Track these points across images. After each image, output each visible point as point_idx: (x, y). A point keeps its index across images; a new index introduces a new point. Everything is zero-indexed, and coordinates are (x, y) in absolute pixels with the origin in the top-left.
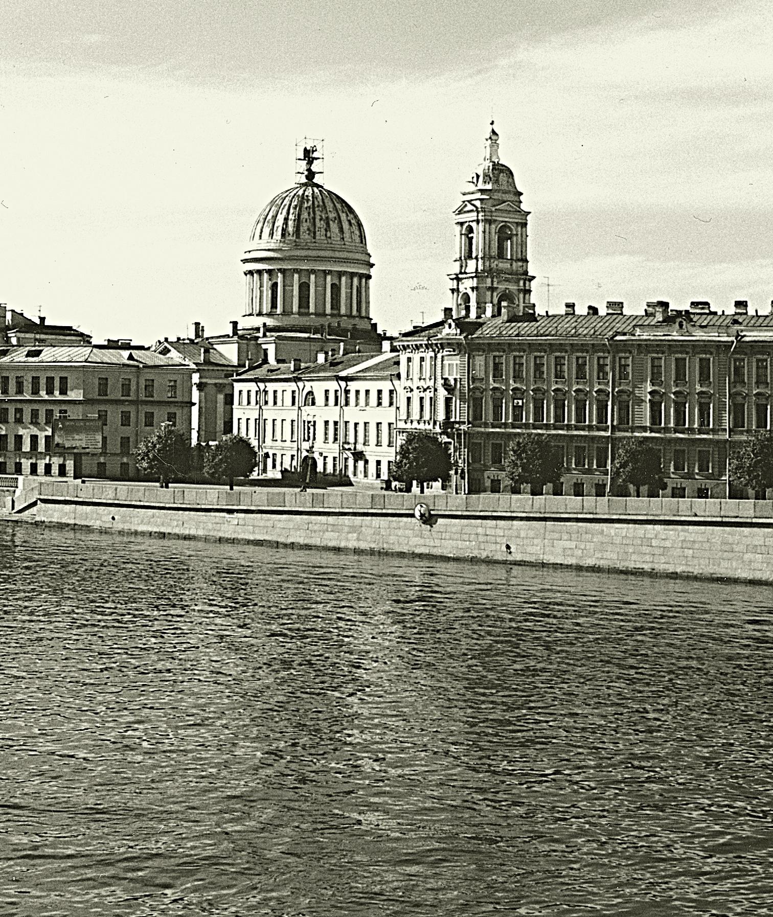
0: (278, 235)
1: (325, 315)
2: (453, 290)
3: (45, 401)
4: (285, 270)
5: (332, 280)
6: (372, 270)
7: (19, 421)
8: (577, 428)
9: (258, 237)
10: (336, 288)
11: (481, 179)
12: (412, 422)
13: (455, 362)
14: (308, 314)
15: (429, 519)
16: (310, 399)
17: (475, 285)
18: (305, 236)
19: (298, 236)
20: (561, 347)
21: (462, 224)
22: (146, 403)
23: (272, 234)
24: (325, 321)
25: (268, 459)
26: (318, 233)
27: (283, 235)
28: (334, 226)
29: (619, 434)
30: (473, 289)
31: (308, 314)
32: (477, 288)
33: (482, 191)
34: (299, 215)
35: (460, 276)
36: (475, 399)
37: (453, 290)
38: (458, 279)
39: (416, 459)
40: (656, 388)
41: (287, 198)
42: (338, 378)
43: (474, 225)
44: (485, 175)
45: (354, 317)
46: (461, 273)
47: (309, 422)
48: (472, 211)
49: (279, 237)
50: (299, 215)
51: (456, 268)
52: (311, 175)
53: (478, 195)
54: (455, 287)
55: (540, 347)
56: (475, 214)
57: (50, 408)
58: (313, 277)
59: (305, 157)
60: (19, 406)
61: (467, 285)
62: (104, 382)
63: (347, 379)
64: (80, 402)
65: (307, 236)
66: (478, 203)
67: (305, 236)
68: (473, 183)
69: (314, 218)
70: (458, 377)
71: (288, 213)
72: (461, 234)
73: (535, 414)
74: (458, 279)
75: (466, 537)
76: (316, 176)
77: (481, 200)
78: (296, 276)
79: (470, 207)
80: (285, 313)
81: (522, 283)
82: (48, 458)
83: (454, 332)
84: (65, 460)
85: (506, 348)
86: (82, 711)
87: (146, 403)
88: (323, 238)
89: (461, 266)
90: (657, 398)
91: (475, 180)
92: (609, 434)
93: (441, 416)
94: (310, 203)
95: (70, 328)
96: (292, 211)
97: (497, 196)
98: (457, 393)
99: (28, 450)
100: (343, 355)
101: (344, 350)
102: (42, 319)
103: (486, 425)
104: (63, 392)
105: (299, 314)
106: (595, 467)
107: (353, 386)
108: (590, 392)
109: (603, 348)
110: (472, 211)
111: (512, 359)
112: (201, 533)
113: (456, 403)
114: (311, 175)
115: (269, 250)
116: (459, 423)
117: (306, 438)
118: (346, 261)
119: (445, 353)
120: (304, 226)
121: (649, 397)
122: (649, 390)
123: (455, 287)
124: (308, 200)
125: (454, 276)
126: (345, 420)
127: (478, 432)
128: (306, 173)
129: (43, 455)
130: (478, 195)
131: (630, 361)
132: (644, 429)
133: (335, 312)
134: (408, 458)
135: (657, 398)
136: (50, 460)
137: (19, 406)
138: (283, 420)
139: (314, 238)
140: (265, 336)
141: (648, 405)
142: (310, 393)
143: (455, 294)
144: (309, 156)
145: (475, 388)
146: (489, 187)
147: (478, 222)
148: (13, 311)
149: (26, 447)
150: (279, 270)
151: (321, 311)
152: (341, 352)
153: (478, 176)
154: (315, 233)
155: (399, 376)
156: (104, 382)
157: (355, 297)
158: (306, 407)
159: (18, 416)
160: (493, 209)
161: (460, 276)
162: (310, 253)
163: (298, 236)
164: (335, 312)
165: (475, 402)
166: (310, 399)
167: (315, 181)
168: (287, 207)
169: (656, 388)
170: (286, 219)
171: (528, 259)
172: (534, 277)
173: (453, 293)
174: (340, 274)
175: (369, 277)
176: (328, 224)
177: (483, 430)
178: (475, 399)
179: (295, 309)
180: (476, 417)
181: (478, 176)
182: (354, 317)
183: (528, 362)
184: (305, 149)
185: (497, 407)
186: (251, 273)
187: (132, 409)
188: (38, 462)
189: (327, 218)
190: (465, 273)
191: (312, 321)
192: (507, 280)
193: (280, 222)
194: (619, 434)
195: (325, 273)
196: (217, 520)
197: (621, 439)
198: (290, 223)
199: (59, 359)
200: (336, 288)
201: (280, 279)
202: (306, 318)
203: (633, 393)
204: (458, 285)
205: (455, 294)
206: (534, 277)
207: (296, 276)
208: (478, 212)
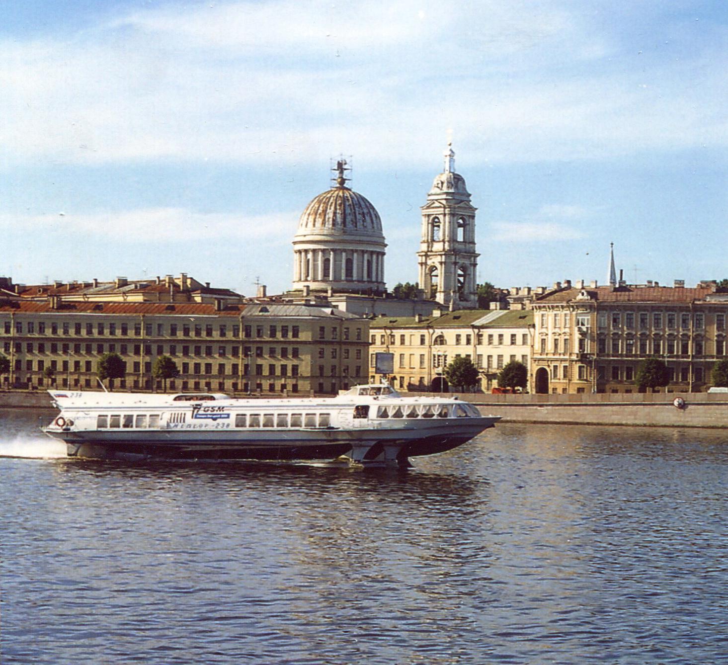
0: (329, 225)
1: (340, 280)
2: (422, 264)
3: (194, 341)
4: (336, 250)
5: (346, 256)
6: (386, 249)
7: (260, 355)
8: (627, 356)
9: (312, 226)
10: (349, 262)
11: (445, 185)
12: (571, 354)
13: (586, 318)
14: (352, 281)
15: (683, 406)
16: (441, 340)
17: (443, 260)
18: (349, 225)
19: (345, 226)
20: (658, 308)
21: (429, 216)
22: (345, 343)
23: (324, 223)
24: (361, 286)
25: (395, 381)
26: (358, 224)
27: (334, 225)
28: (368, 219)
29: (696, 360)
30: (441, 263)
31: (352, 281)
32: (445, 263)
33: (447, 193)
34: (345, 210)
35: (429, 253)
36: (600, 340)
37: (422, 264)
38: (426, 256)
39: (656, 373)
40: (720, 333)
41: (332, 198)
42: (474, 327)
43: (441, 217)
44: (449, 182)
45: (374, 282)
46: (428, 251)
47: (439, 356)
48: (440, 207)
49: (331, 226)
50: (345, 210)
51: (424, 247)
52: (343, 181)
53: (444, 196)
54: (424, 261)
55: (632, 308)
56: (442, 209)
57: (285, 346)
58: (355, 255)
59: (338, 167)
60: (259, 345)
61: (435, 261)
62: (322, 329)
63: (479, 328)
64: (310, 343)
65: (351, 226)
66: (444, 202)
67: (349, 225)
68: (438, 187)
69: (355, 213)
70: (589, 326)
71: (336, 209)
72: (428, 223)
73: (641, 349)
74: (426, 256)
75: (708, 415)
76: (346, 181)
77: (446, 199)
78: (344, 254)
79: (437, 204)
80: (335, 280)
81: (473, 259)
82: (283, 379)
83: (586, 298)
84: (297, 381)
85: (650, 309)
86: (153, 566)
87: (345, 343)
88: (362, 227)
89: (428, 247)
90: (721, 339)
91: (440, 185)
92: (690, 360)
93: (576, 350)
94: (351, 202)
95: (228, 291)
96: (338, 207)
97: (457, 197)
98: (588, 336)
99: (268, 374)
100: (453, 311)
101: (453, 307)
102: (208, 284)
103: (608, 355)
104: (295, 335)
105: (347, 281)
106: (625, 379)
107: (486, 333)
108: (636, 334)
109: (687, 309)
110: (440, 207)
111: (625, 314)
112: (520, 419)
113: (588, 343)
114: (343, 181)
115: (324, 235)
116: (590, 354)
117: (436, 365)
118: (360, 242)
119: (579, 312)
120: (349, 218)
121: (715, 338)
122: (716, 334)
123: (424, 261)
124: (348, 200)
125: (424, 254)
126: (478, 353)
127: (603, 360)
128: (339, 180)
129: (279, 378)
130: (444, 196)
131: (703, 317)
132: (713, 357)
133: (350, 278)
134: (649, 372)
135: (672, 338)
136: (285, 381)
137: (259, 345)
138: (411, 355)
139: (356, 227)
140: (332, 296)
141: (715, 343)
142: (441, 336)
143: (424, 267)
144: (341, 167)
145: (601, 333)
146: (452, 191)
147: (445, 215)
148: (191, 278)
149: (266, 372)
150: (332, 250)
151: (360, 279)
152: (451, 309)
153: (442, 183)
154: (356, 224)
155: (534, 326)
156: (322, 329)
157: (365, 268)
158: (436, 346)
159: (259, 352)
160: (457, 206)
161: (429, 253)
162: (352, 238)
163: (345, 226)
164: (350, 278)
165: (601, 341)
166: (441, 340)
167: (345, 185)
168: (333, 204)
169: (720, 333)
170: (335, 213)
171: (476, 242)
172: (479, 255)
173: (422, 266)
174: (372, 253)
175: (384, 254)
176: (364, 217)
177: (606, 358)
178: (600, 340)
179: (343, 278)
180: (602, 350)
181: (442, 183)
182: (374, 282)
183: (678, 317)
184: (339, 162)
185: (615, 346)
186: (300, 252)
187: (337, 347)
188: (276, 382)
189: (363, 213)
190: (432, 251)
191: (355, 285)
192: (464, 257)
193: (330, 215)
194: (696, 360)
195: (363, 252)
196: (532, 411)
197: (696, 363)
198: (338, 216)
199: (288, 314)
200: (349, 262)
201: (310, 256)
202: (351, 284)
203: (705, 336)
204: (426, 259)
205: (424, 267)
206: (479, 255)
207: (344, 254)
208: (445, 208)
